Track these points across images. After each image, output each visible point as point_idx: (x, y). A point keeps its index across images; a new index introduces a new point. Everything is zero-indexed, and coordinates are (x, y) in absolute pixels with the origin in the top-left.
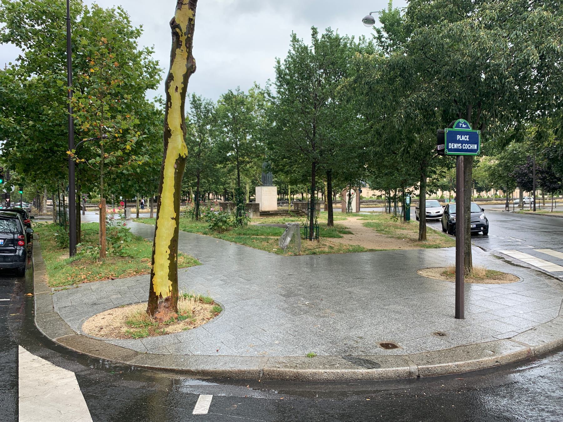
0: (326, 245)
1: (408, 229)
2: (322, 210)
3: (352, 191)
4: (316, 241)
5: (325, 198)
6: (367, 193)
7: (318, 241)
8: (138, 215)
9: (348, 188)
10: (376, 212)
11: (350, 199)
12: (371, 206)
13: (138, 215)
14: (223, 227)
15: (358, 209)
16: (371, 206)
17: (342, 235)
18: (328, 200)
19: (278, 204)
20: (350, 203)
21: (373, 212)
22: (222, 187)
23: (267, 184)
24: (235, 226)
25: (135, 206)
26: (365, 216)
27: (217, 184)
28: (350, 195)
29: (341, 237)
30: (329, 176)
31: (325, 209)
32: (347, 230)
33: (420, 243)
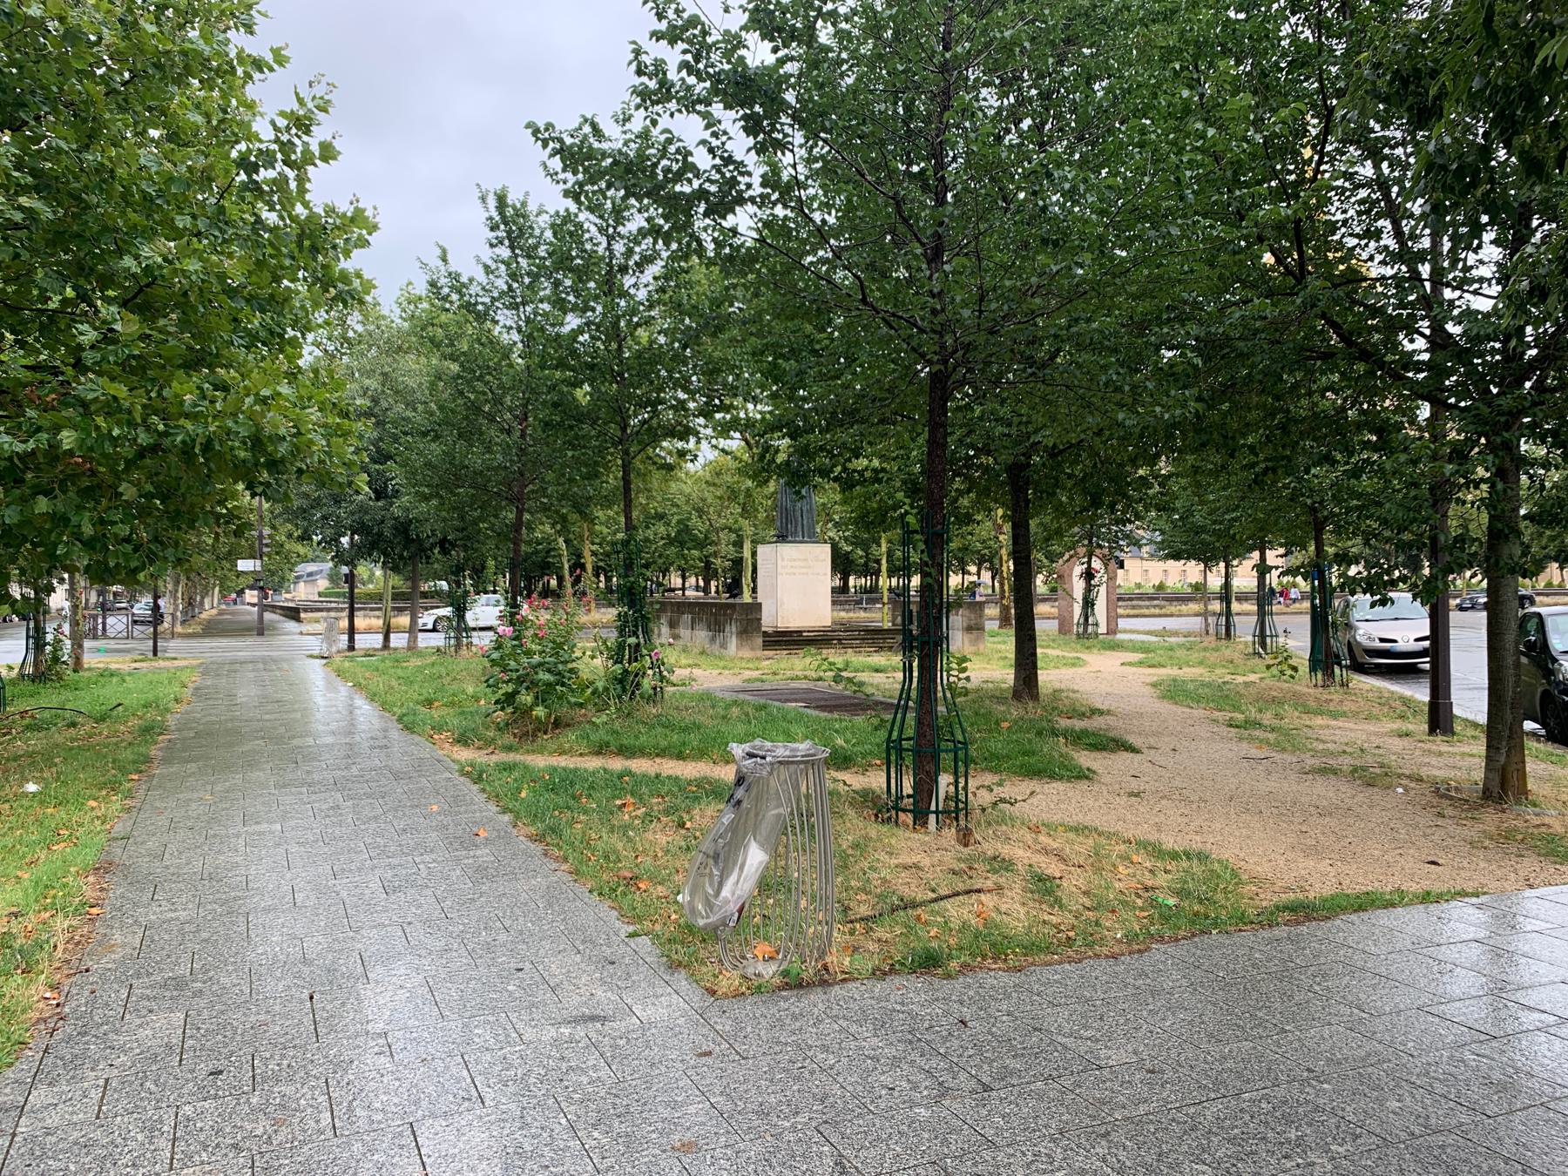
0: (1006, 865)
1: (1355, 714)
2: (992, 626)
3: (1096, 564)
4: (950, 833)
5: (1002, 585)
6: (1143, 570)
7: (965, 838)
8: (351, 640)
9: (1082, 551)
10: (1175, 634)
11: (1089, 589)
12: (1153, 611)
13: (351, 640)
14: (540, 712)
15: (1112, 618)
16: (1146, 611)
17: (1085, 759)
18: (921, 688)
19: (834, 603)
20: (1088, 603)
21: (1163, 633)
22: (695, 553)
23: (795, 534)
24: (599, 699)
25: (379, 609)
26: (1145, 649)
27: (682, 544)
28: (1089, 575)
29: (1084, 775)
30: (1020, 489)
31: (1004, 620)
32: (1096, 723)
33: (1490, 819)
